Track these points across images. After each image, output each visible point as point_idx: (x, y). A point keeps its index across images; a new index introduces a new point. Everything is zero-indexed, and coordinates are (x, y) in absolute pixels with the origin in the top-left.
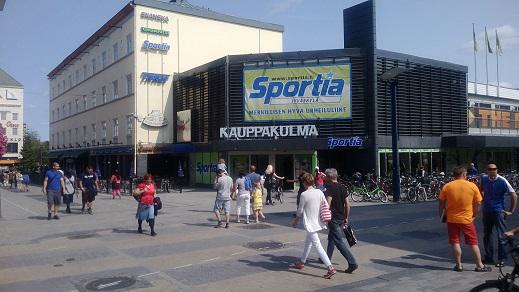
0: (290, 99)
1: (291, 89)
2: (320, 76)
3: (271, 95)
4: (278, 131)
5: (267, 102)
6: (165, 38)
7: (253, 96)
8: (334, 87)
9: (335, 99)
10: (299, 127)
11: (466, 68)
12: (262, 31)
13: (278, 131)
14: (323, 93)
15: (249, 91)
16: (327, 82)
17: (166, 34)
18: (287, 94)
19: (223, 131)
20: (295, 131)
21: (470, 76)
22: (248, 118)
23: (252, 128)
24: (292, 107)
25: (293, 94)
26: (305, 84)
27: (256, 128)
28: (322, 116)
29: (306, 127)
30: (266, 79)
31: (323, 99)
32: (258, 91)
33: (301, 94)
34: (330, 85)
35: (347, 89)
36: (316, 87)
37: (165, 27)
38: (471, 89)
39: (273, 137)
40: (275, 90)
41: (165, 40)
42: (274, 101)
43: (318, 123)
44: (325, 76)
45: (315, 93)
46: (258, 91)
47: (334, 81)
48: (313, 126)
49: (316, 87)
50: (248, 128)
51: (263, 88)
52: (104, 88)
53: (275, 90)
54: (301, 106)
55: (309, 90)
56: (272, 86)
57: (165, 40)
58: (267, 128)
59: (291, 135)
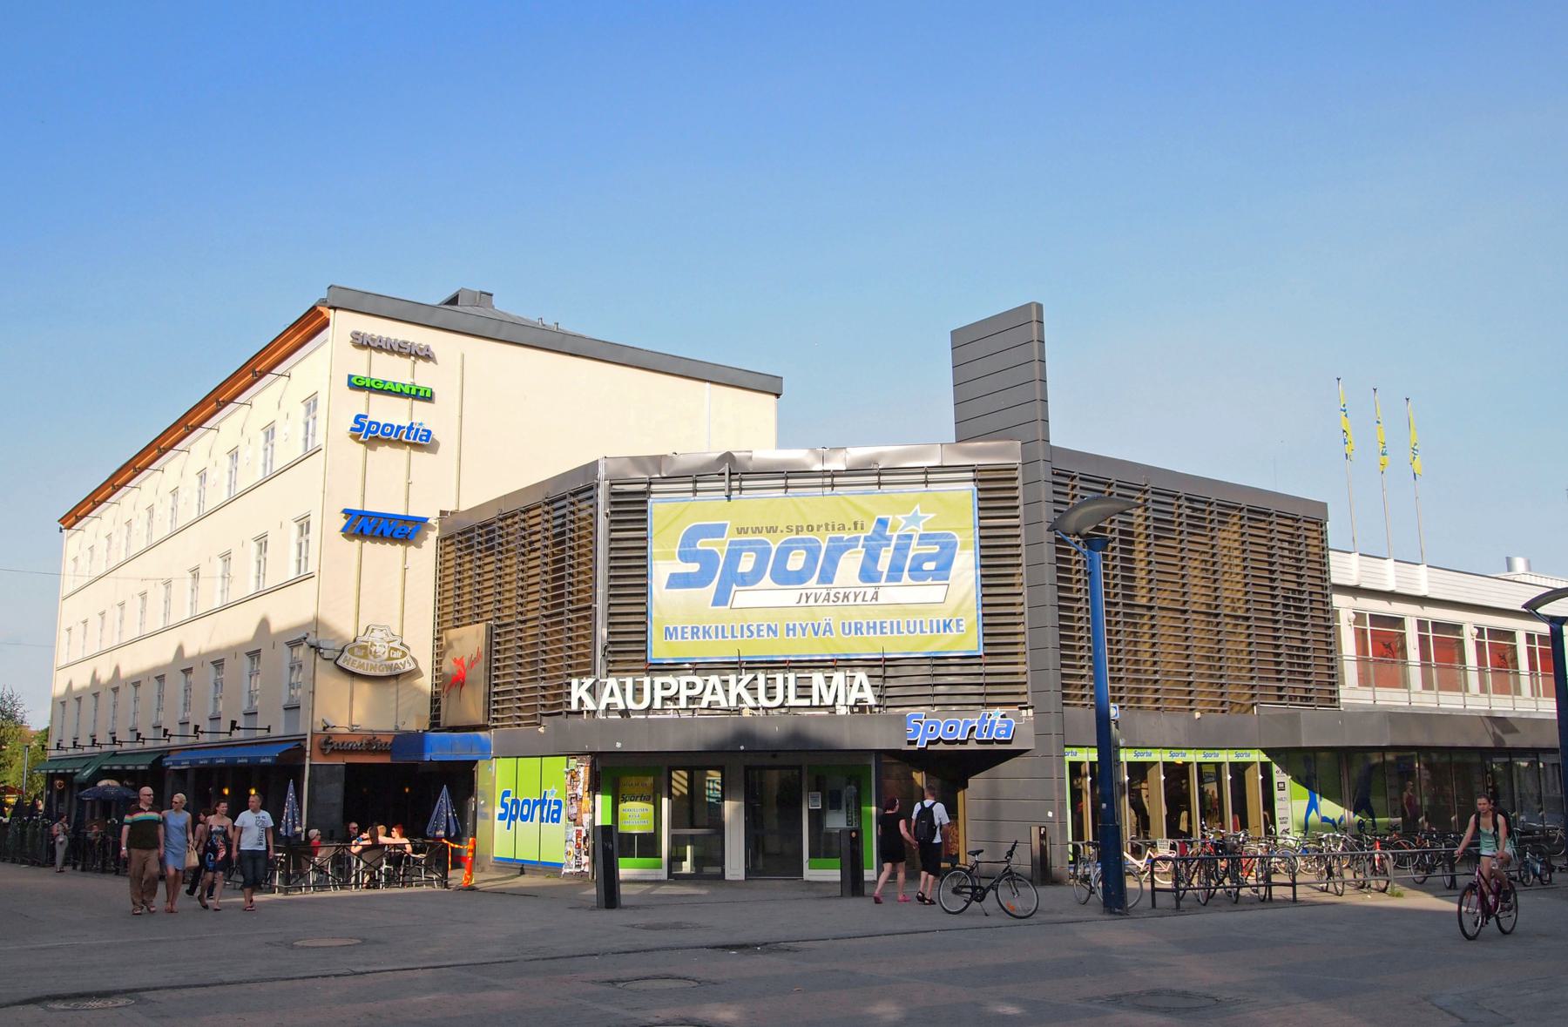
0: (788, 596)
1: (796, 562)
2: (883, 523)
3: (733, 579)
4: (752, 689)
5: (721, 598)
6: (361, 372)
7: (677, 581)
8: (930, 558)
9: (930, 592)
10: (818, 678)
11: (1323, 506)
12: (401, 512)
13: (752, 689)
14: (895, 573)
15: (662, 568)
16: (418, 430)
17: (355, 385)
18: (785, 578)
19: (578, 690)
20: (804, 689)
21: (1335, 532)
22: (660, 650)
23: (669, 679)
24: (799, 618)
25: (799, 578)
26: (838, 549)
27: (684, 679)
28: (895, 647)
29: (839, 677)
30: (718, 531)
31: (891, 593)
32: (694, 567)
33: (827, 577)
34: (915, 549)
35: (966, 565)
36: (872, 556)
37: (424, 375)
38: (1344, 569)
39: (739, 711)
40: (746, 564)
41: (422, 414)
42: (742, 597)
43: (881, 668)
44: (899, 524)
45: (868, 574)
46: (694, 567)
47: (423, 430)
48: (861, 676)
49: (872, 556)
50: (659, 680)
51: (708, 559)
52: (122, 605)
53: (746, 564)
54: (828, 614)
55: (849, 566)
56: (734, 555)
57: (422, 414)
58: (714, 679)
59: (792, 701)
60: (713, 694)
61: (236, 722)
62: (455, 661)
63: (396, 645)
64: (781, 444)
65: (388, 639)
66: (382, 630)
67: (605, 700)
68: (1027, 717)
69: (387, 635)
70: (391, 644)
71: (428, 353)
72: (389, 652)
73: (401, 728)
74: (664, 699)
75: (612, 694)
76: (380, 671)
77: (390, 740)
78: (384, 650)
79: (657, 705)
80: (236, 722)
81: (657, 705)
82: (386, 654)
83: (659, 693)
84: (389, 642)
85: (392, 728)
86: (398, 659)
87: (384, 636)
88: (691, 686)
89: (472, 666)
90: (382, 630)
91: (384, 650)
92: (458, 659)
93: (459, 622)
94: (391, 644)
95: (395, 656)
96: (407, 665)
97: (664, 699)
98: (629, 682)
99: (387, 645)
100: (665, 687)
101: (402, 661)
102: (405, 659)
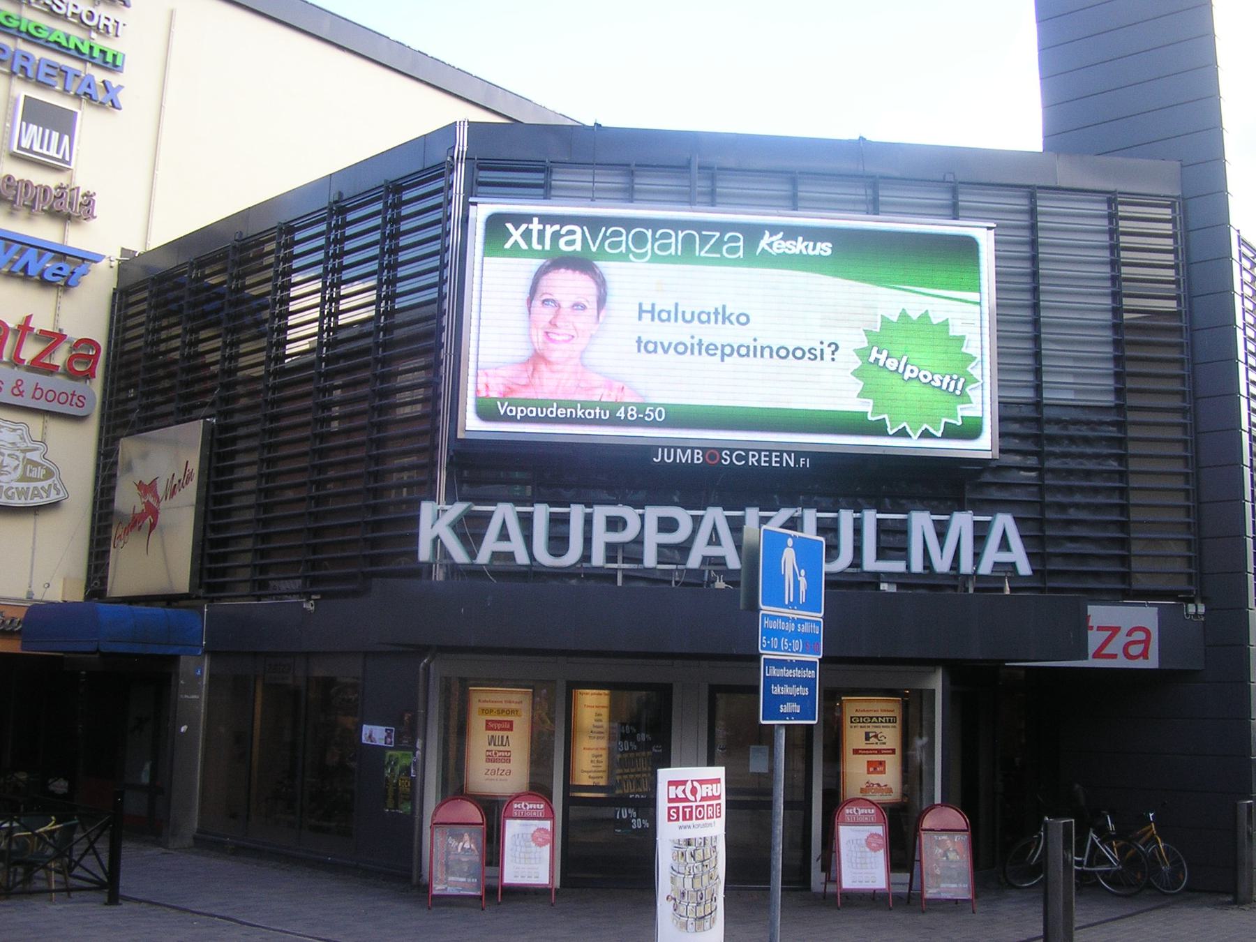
27: (653, 513)
50: (601, 513)
59: (871, 563)
60: (710, 543)
61: (862, 789)
62: (140, 485)
63: (35, 456)
64: (22, 649)
65: (23, 446)
66: (14, 430)
67: (490, 545)
68: (1196, 614)
69: (22, 438)
70: (29, 455)
71: (88, 91)
72: (25, 468)
73: (38, 596)
74: (611, 548)
75: (504, 535)
76: (8, 497)
77: (20, 615)
78: (17, 462)
79: (598, 559)
80: (862, 789)
81: (598, 559)
82: (19, 471)
83: (601, 537)
84: (24, 451)
85: (23, 595)
86: (40, 480)
87: (17, 439)
88: (667, 525)
89: (173, 493)
90: (14, 430)
91: (17, 462)
92: (147, 482)
93: (148, 421)
94: (29, 455)
95: (34, 475)
96: (53, 492)
97: (611, 548)
98: (541, 513)
99: (21, 456)
100: (615, 524)
101: (46, 484)
102: (50, 482)
